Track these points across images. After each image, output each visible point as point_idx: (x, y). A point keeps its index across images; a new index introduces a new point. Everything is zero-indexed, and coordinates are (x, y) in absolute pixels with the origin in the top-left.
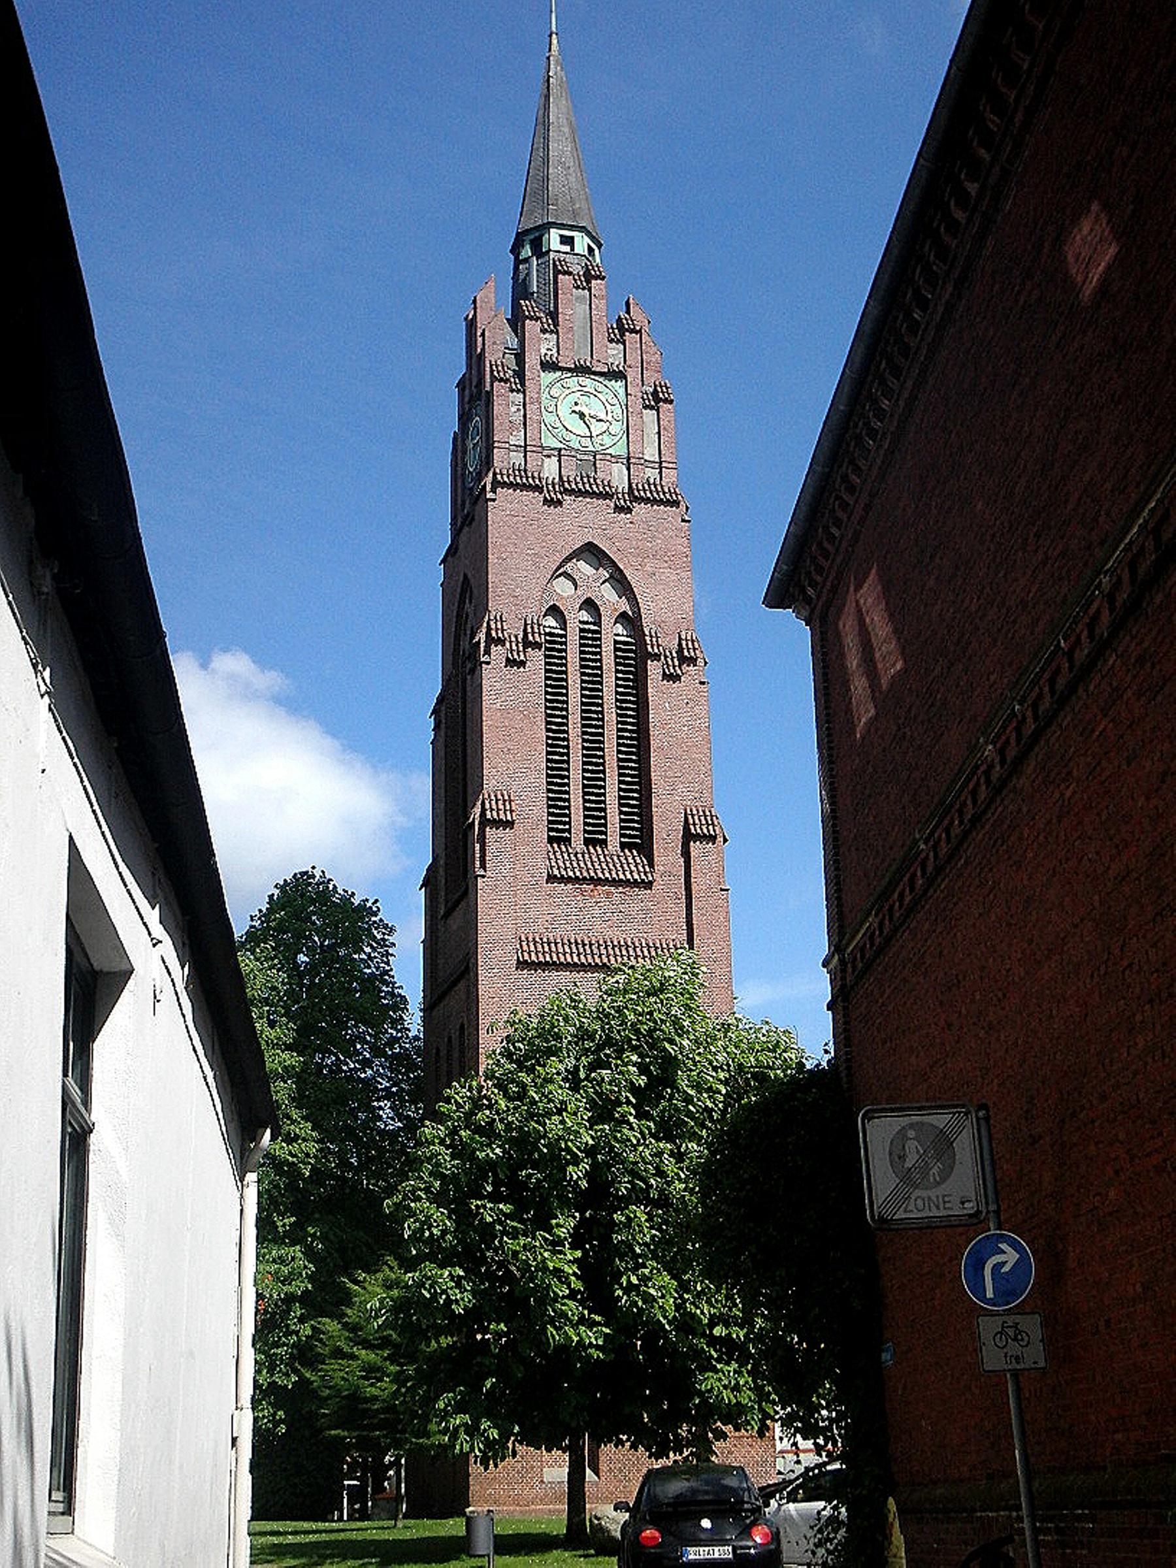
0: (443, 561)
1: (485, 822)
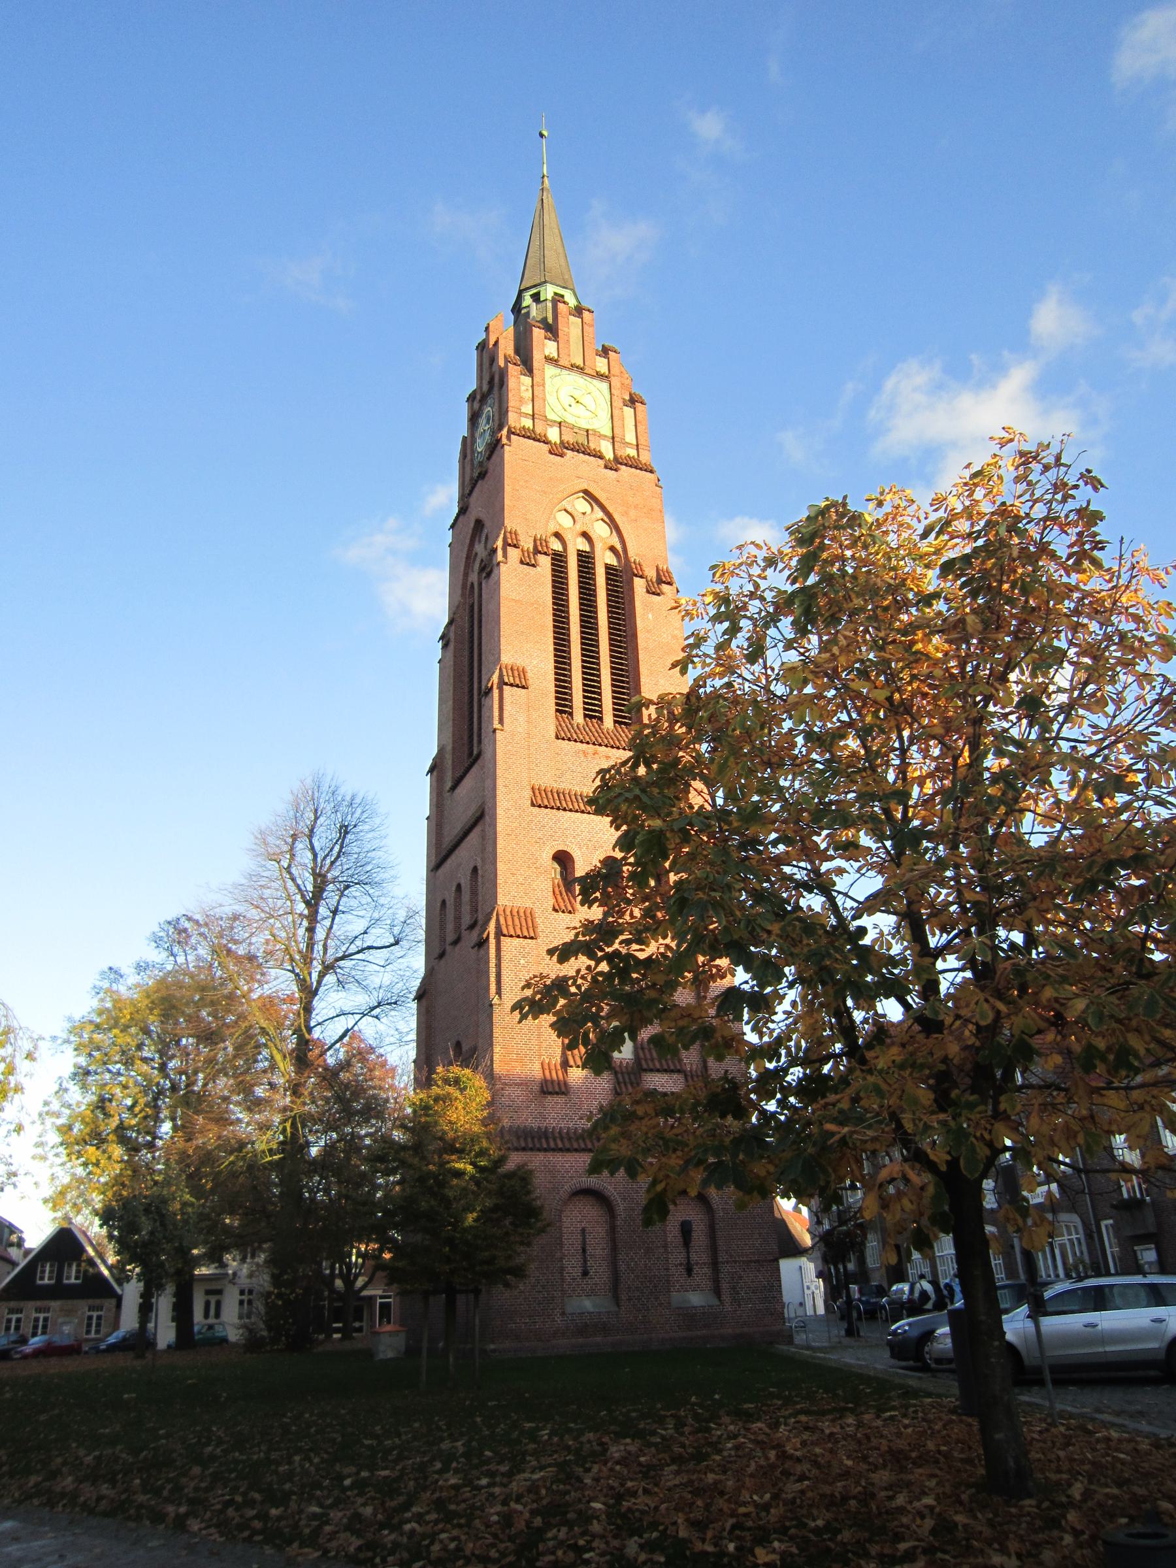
0: (452, 527)
1: (502, 683)
